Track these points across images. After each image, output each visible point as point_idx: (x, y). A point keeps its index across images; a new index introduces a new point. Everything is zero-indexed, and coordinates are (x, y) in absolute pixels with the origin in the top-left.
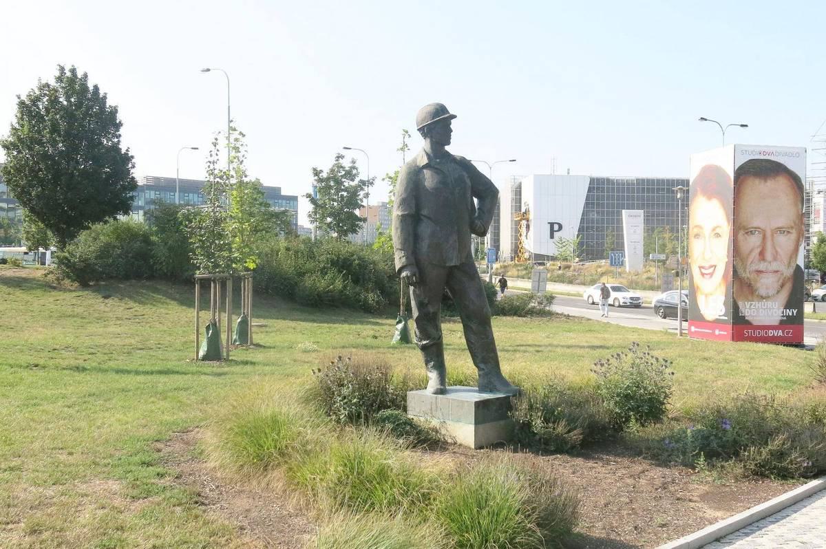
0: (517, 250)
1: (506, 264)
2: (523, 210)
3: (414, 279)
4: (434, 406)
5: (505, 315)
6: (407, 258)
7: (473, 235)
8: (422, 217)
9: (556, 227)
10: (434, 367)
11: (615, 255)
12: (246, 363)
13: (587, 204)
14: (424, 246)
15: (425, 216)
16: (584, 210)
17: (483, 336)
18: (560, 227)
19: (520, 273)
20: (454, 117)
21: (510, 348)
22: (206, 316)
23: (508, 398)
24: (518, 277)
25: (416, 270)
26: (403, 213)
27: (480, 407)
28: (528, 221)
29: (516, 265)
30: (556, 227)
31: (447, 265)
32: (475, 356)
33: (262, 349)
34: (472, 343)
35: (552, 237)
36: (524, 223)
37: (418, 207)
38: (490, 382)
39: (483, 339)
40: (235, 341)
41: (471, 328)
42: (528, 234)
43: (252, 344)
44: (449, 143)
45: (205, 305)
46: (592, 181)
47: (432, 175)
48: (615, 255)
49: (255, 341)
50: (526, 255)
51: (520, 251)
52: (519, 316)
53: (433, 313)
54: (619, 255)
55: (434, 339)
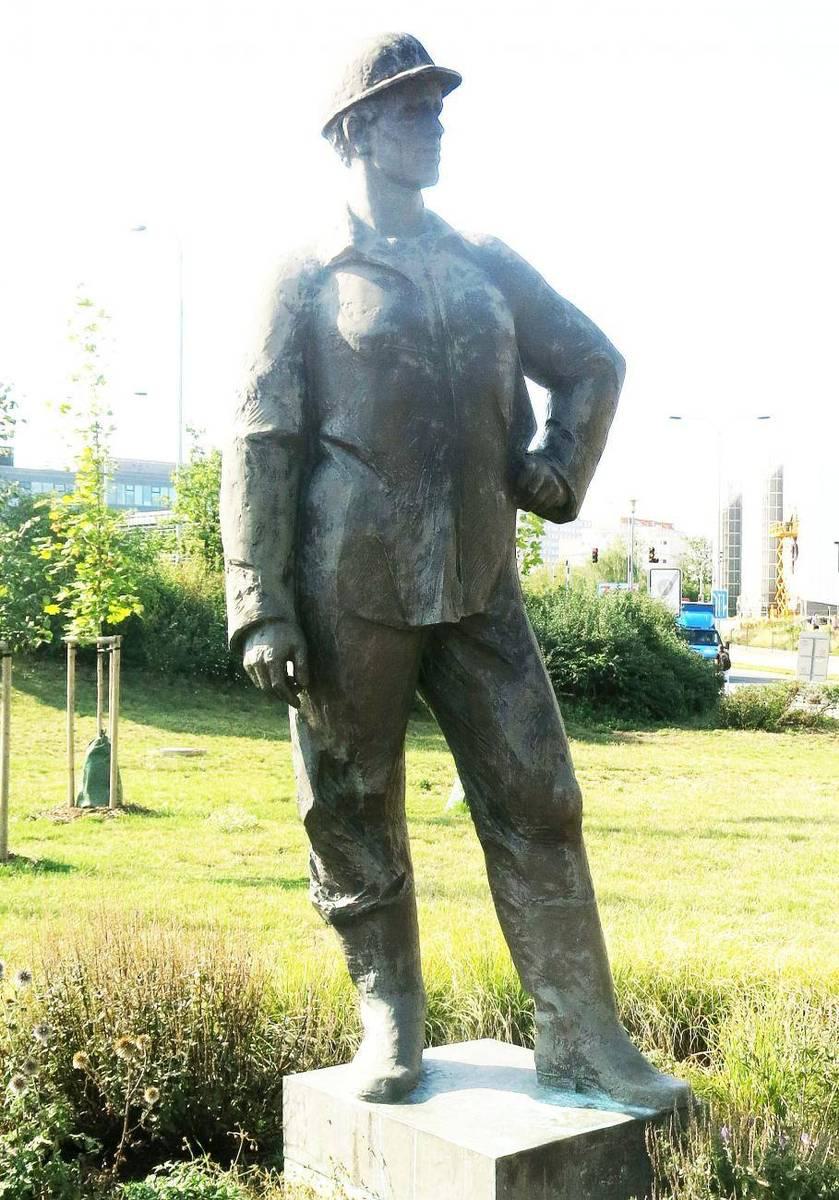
0: (775, 598)
1: (751, 621)
2: (786, 519)
3: (290, 665)
4: (363, 1147)
5: (738, 726)
6: (263, 596)
7: (520, 512)
10: (381, 990)
12: (49, 867)
14: (332, 542)
15: (335, 442)
17: (550, 886)
19: (778, 640)
20: (448, 81)
21: (728, 828)
22: (88, 729)
23: (635, 1127)
24: (774, 646)
25: (294, 638)
26: (255, 429)
27: (523, 1179)
28: (795, 539)
29: (771, 624)
31: (414, 622)
32: (526, 957)
33: (139, 818)
34: (512, 909)
36: (788, 543)
37: (313, 412)
38: (575, 1059)
39: (551, 895)
40: (81, 798)
41: (511, 855)
43: (119, 805)
45: (86, 703)
47: (365, 290)
49: (128, 798)
50: (791, 605)
51: (780, 596)
52: (768, 731)
53: (367, 797)
55: (373, 890)
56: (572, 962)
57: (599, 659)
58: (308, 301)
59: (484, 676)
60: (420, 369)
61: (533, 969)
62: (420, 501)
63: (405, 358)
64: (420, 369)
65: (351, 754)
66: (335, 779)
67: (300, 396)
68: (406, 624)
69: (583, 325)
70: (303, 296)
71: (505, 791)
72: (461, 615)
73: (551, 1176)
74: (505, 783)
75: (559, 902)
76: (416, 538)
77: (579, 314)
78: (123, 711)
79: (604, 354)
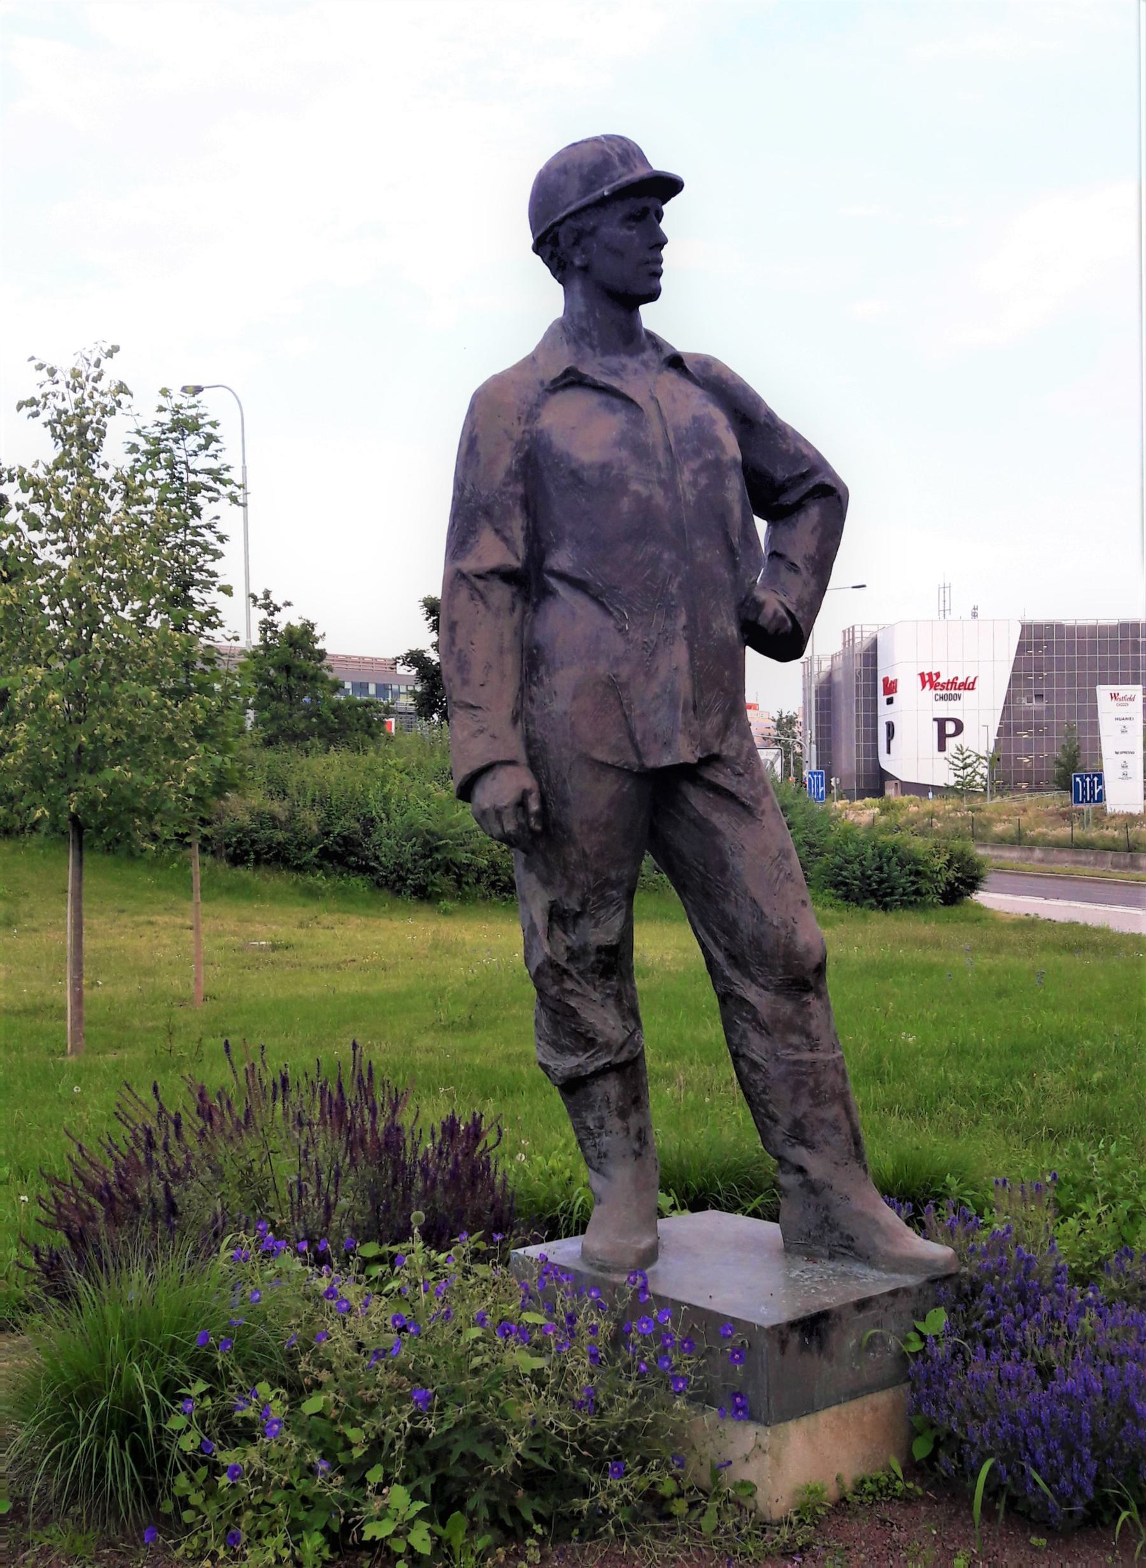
8: (553, 582)
9: (950, 728)
11: (1084, 781)
13: (1015, 679)
15: (562, 576)
16: (1009, 691)
18: (959, 727)
20: (669, 186)
30: (950, 728)
35: (942, 747)
42: (892, 742)
44: (653, 295)
46: (1026, 629)
48: (1084, 781)
54: (1092, 781)
56: (822, 1121)
57: (258, 919)
58: (527, 427)
59: (720, 819)
60: (650, 497)
61: (779, 1128)
62: (653, 637)
63: (634, 486)
64: (650, 497)
65: (583, 904)
66: (565, 932)
67: (522, 529)
68: (642, 765)
69: (805, 451)
70: (523, 420)
71: (745, 938)
72: (698, 754)
73: (821, 1347)
74: (745, 931)
75: (807, 1056)
76: (650, 674)
77: (798, 437)
78: (205, 899)
79: (828, 481)
